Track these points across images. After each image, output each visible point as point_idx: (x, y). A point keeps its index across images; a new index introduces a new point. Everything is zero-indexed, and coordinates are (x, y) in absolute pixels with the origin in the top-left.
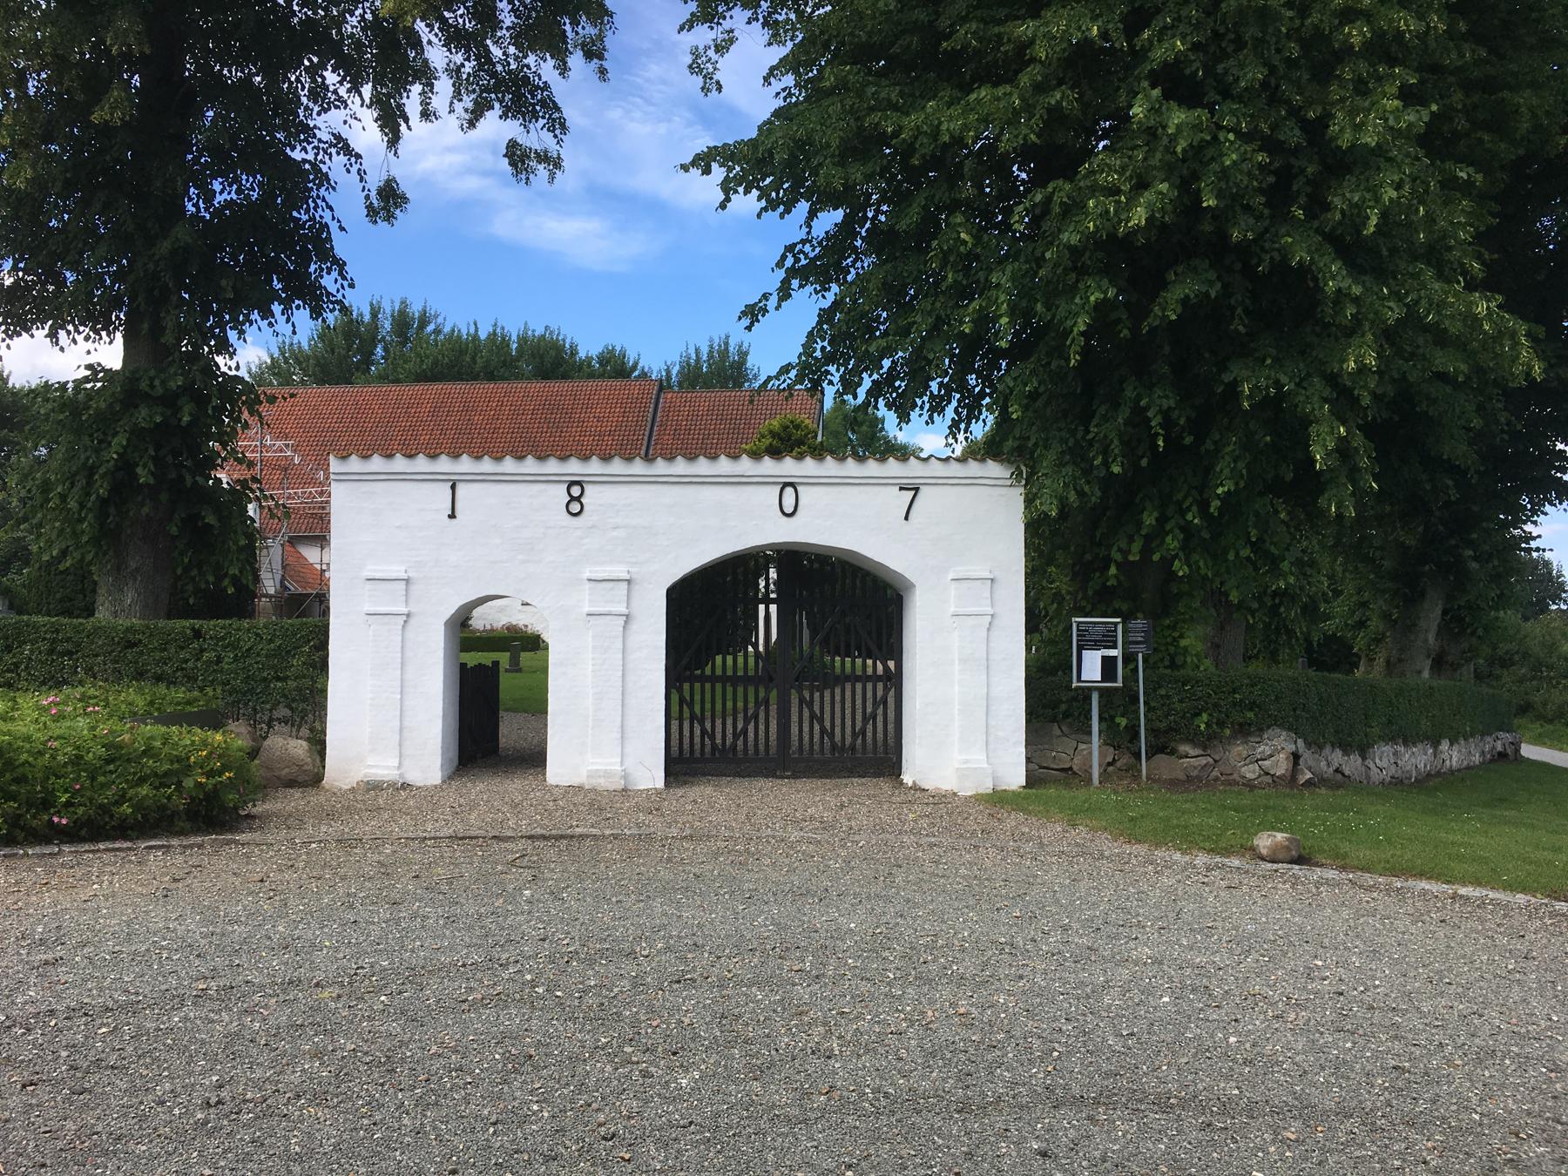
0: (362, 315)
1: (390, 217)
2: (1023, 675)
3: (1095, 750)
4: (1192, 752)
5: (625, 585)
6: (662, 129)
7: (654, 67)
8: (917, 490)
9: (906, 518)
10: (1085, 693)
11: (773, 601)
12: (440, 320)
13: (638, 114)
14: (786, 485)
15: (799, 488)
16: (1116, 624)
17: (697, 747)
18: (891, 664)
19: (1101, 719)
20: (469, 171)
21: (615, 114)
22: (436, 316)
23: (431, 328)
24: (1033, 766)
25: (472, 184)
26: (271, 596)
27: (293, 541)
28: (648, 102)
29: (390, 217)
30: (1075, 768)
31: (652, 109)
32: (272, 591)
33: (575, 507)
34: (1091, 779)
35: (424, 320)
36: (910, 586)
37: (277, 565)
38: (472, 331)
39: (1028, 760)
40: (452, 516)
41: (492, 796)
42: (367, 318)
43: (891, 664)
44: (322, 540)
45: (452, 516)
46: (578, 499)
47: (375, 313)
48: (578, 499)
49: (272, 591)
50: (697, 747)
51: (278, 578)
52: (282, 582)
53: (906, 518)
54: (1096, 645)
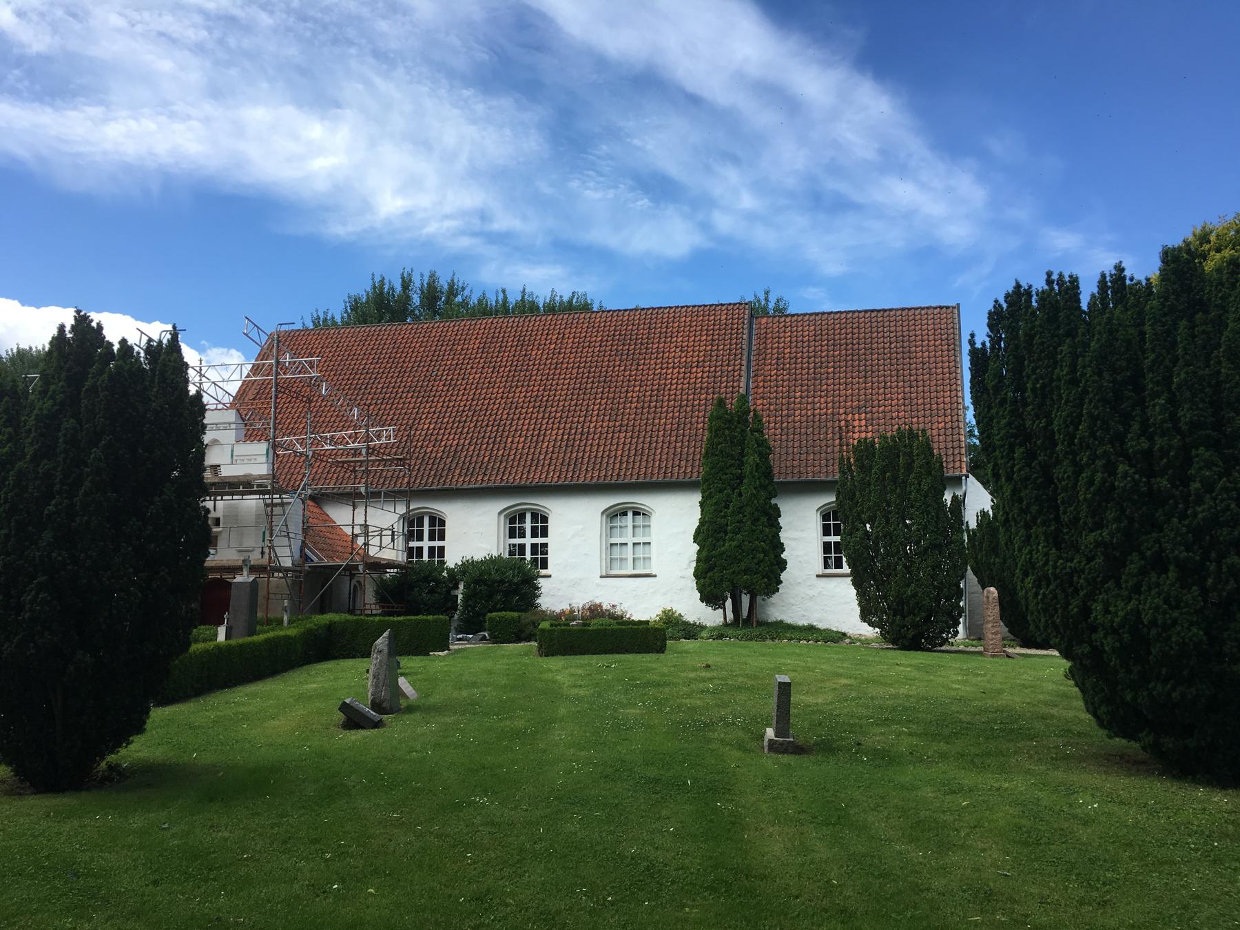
0: (392, 289)
4: (928, 792)
6: (611, 194)
7: (605, 147)
12: (466, 292)
13: (592, 184)
20: (463, 233)
21: (574, 184)
22: (463, 289)
23: (459, 299)
25: (465, 242)
26: (287, 570)
27: (319, 499)
28: (601, 174)
31: (602, 179)
32: (287, 563)
35: (452, 291)
37: (296, 527)
38: (501, 296)
42: (398, 288)
44: (827, 547)
47: (406, 284)
49: (287, 563)
51: (296, 545)
52: (302, 550)
53: (818, 576)
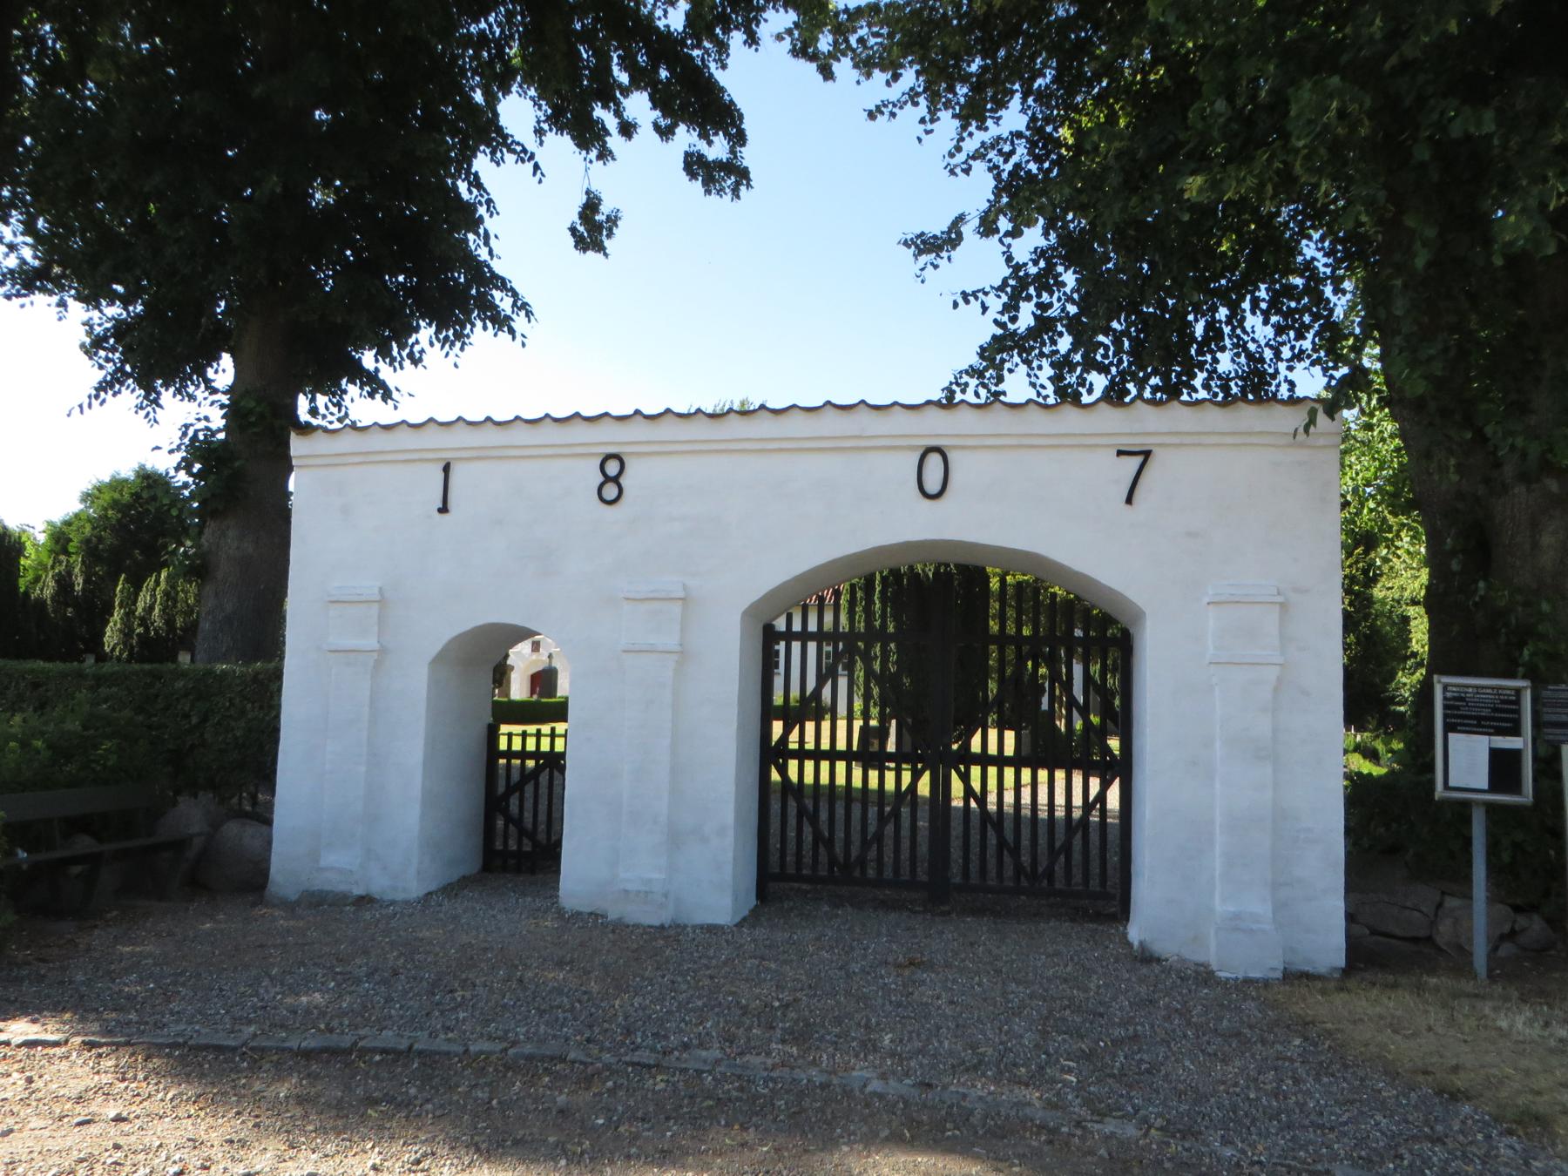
1: (600, 248)
2: (982, 541)
3: (1479, 914)
5: (676, 608)
8: (1147, 454)
9: (1129, 500)
10: (1461, 810)
11: (891, 638)
14: (930, 450)
15: (951, 456)
16: (1518, 691)
17: (807, 860)
18: (775, 776)
19: (1493, 868)
24: (1357, 929)
29: (600, 248)
30: (1440, 941)
33: (610, 491)
34: (1465, 953)
36: (1139, 615)
39: (1350, 917)
40: (444, 509)
41: (502, 919)
43: (775, 776)
45: (444, 509)
46: (616, 480)
48: (608, 479)
50: (807, 860)
53: (1129, 500)
54: (1477, 724)
